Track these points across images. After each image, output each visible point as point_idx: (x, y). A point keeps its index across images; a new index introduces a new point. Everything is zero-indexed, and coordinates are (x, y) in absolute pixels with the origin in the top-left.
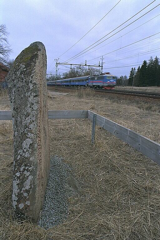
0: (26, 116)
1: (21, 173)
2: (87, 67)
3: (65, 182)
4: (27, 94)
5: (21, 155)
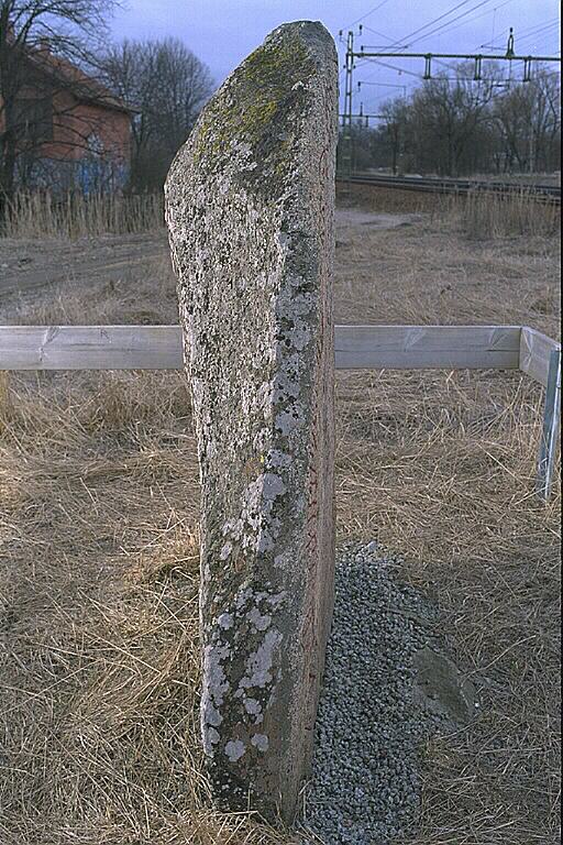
0: (257, 374)
1: (235, 618)
2: (518, 67)
3: (404, 673)
4: (266, 277)
5: (235, 543)
